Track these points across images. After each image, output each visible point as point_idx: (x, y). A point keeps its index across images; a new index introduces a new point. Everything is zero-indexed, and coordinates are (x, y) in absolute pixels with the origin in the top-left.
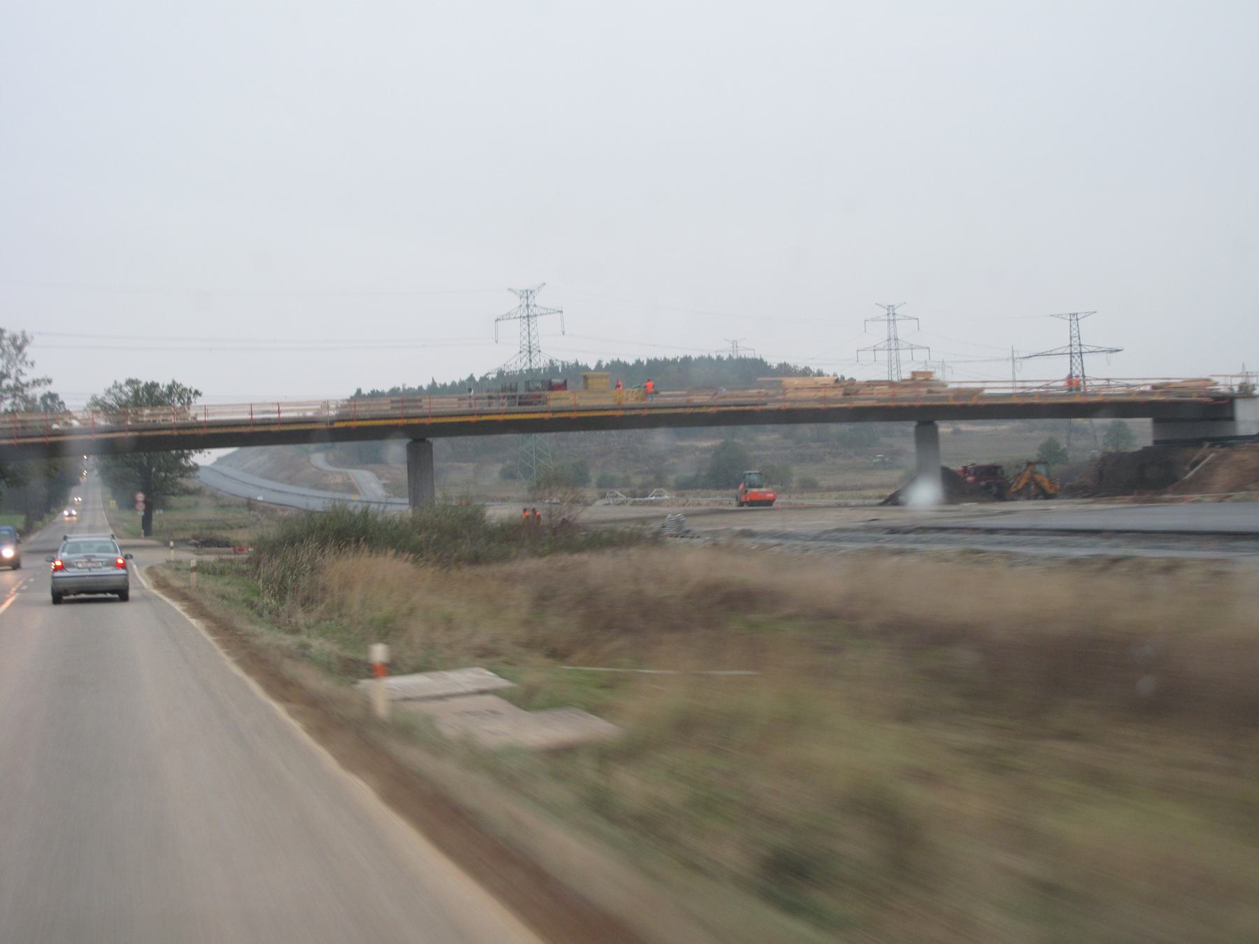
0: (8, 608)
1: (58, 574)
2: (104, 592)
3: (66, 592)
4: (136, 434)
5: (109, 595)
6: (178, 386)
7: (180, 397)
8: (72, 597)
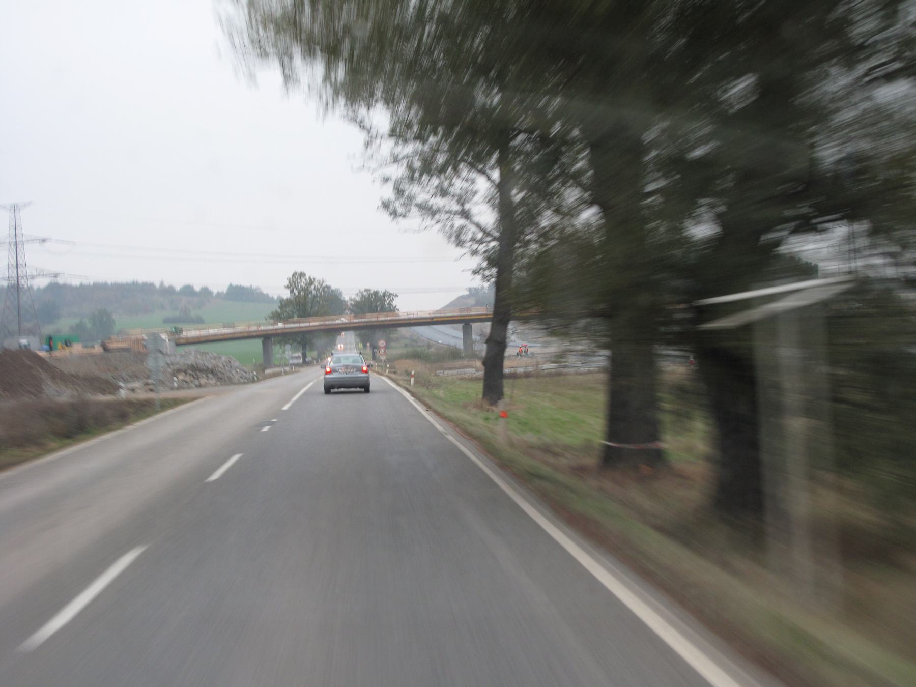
0: (303, 388)
1: (328, 376)
2: (356, 387)
3: (333, 387)
4: (435, 40)
5: (358, 389)
6: (388, 293)
7: (389, 297)
8: (336, 390)
